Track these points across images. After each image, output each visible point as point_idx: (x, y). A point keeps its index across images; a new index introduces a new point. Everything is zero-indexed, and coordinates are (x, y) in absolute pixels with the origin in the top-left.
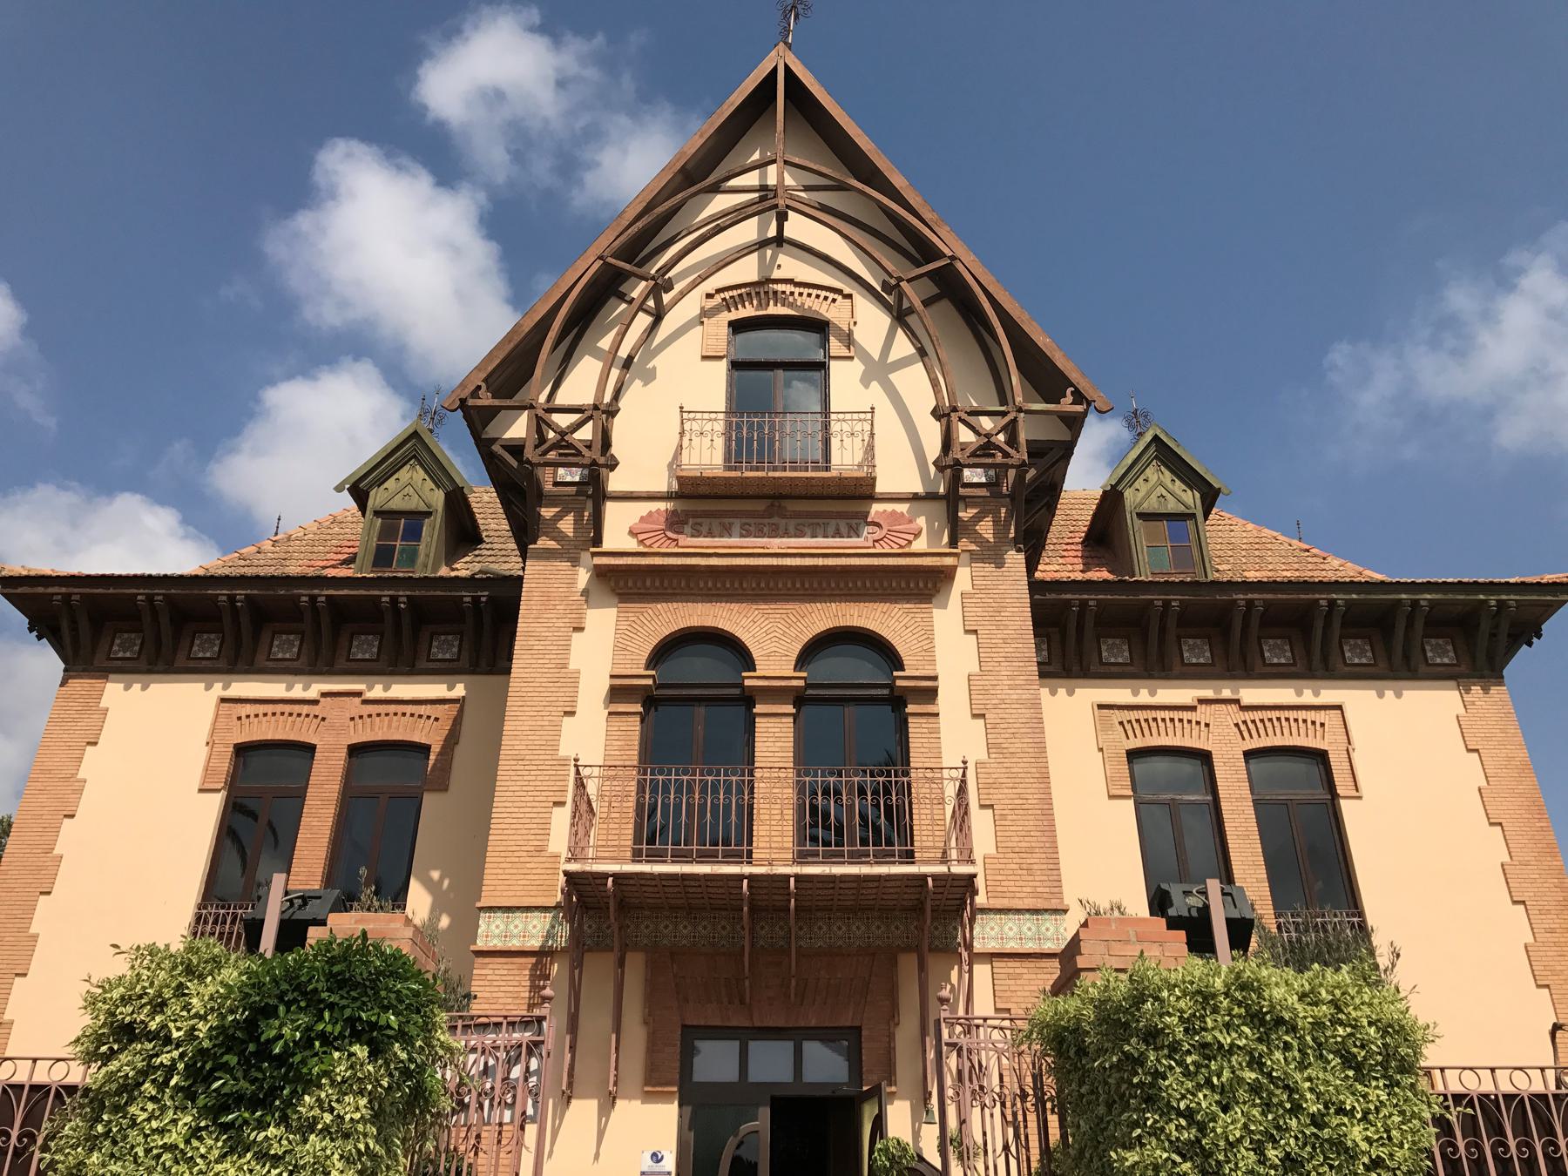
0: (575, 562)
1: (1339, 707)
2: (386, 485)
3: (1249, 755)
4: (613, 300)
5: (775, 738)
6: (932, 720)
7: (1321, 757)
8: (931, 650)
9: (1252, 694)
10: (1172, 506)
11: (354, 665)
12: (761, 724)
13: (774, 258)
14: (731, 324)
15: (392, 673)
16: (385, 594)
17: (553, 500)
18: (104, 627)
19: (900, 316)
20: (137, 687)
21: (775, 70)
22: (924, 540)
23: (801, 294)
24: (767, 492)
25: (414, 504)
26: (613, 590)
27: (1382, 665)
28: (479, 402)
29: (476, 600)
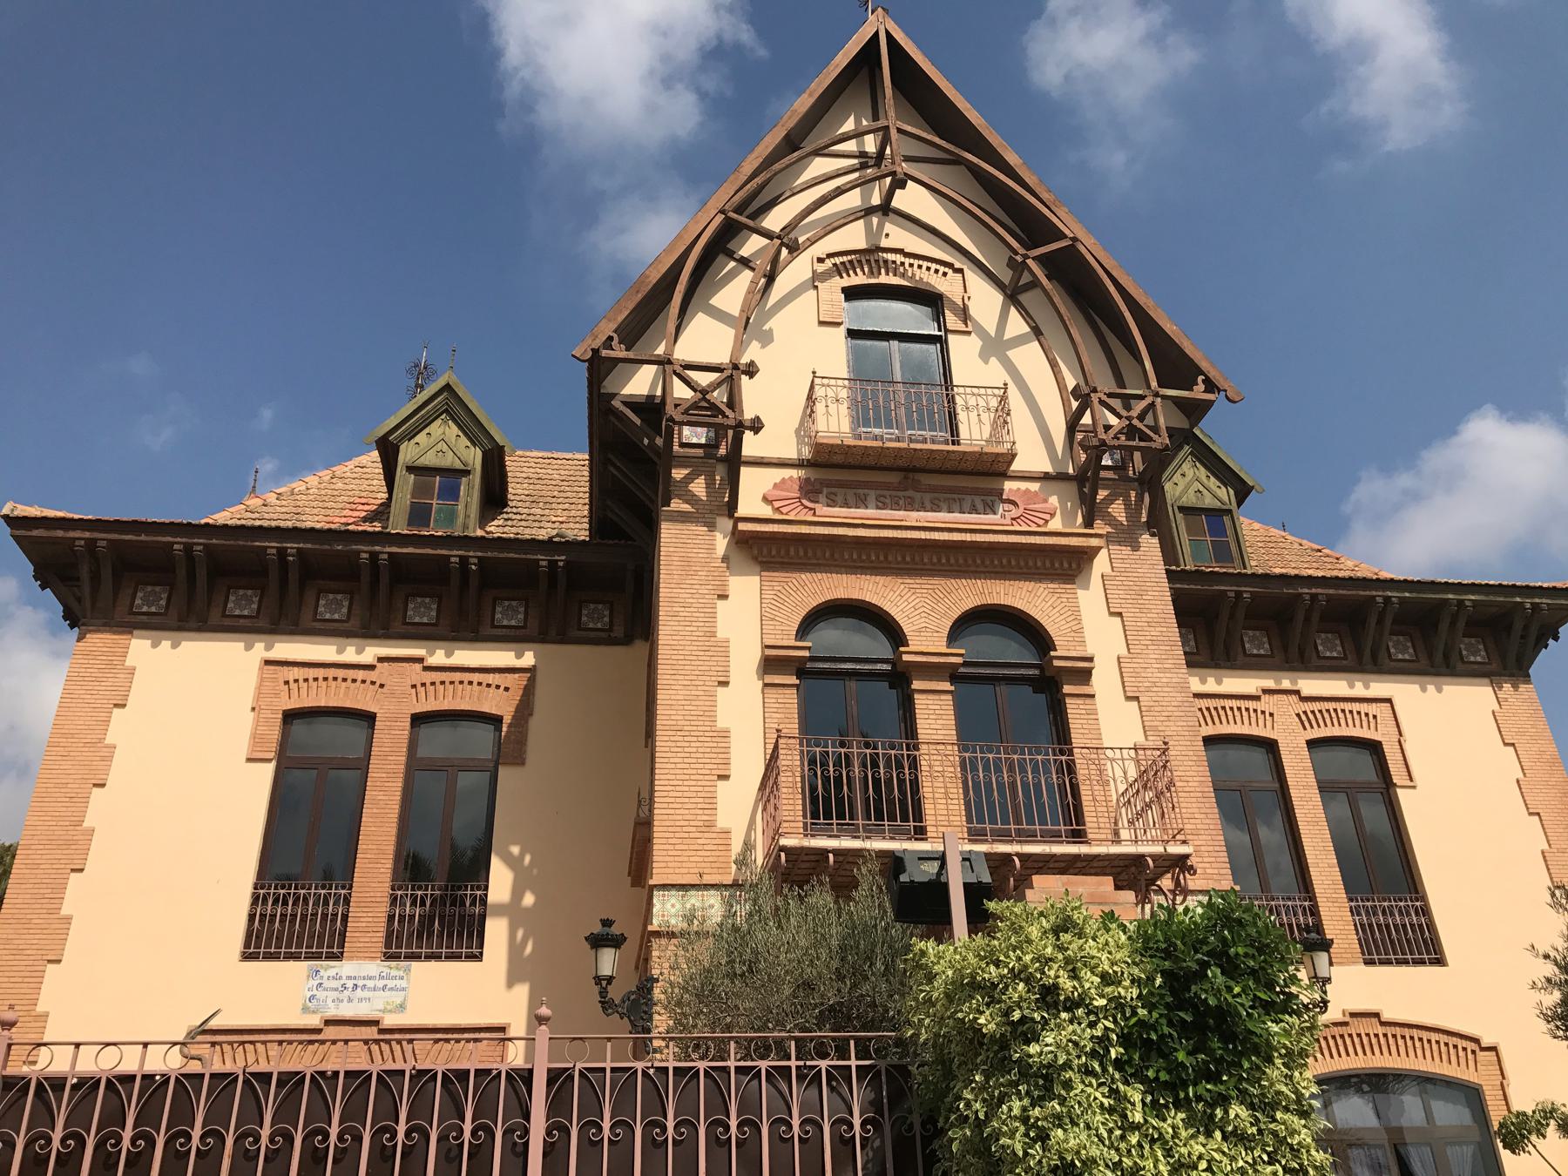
0: (712, 526)
1: (1389, 701)
2: (417, 439)
3: (1312, 744)
4: (721, 258)
5: (935, 715)
6: (1088, 701)
7: (1375, 748)
8: (1080, 631)
9: (1312, 685)
10: (1208, 502)
11: (411, 629)
12: (919, 700)
13: (881, 226)
14: (844, 290)
15: (454, 639)
16: (455, 554)
17: (683, 462)
18: (118, 577)
19: (1012, 295)
20: (166, 644)
21: (877, 33)
22: (1058, 519)
23: (911, 265)
24: (901, 467)
25: (448, 461)
26: (755, 559)
27: (1424, 661)
28: (612, 354)
29: (553, 564)
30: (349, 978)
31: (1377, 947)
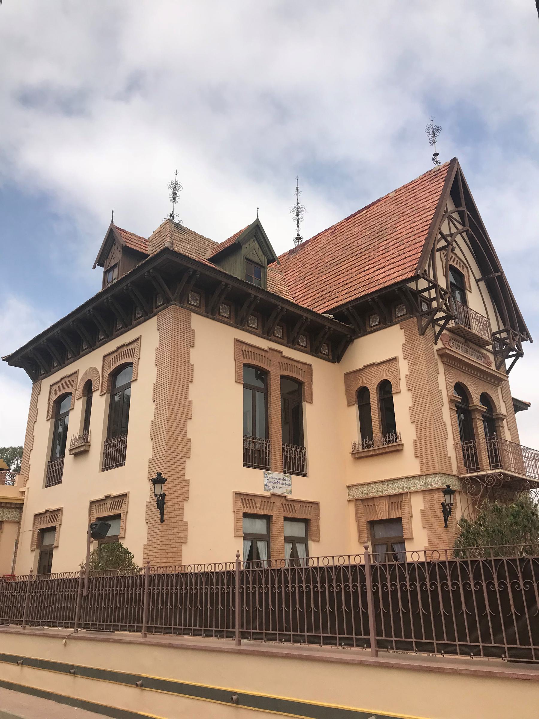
3: (282, 377)
30: (275, 478)
31: (298, 468)
